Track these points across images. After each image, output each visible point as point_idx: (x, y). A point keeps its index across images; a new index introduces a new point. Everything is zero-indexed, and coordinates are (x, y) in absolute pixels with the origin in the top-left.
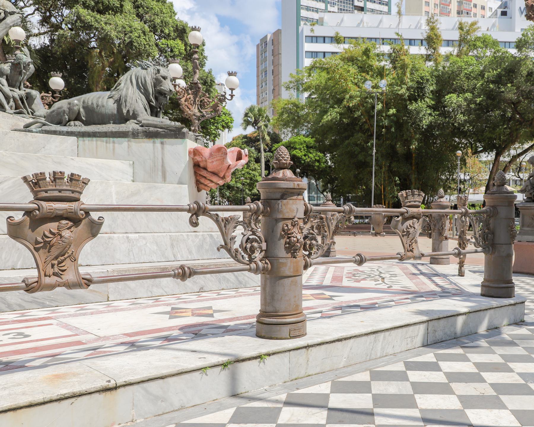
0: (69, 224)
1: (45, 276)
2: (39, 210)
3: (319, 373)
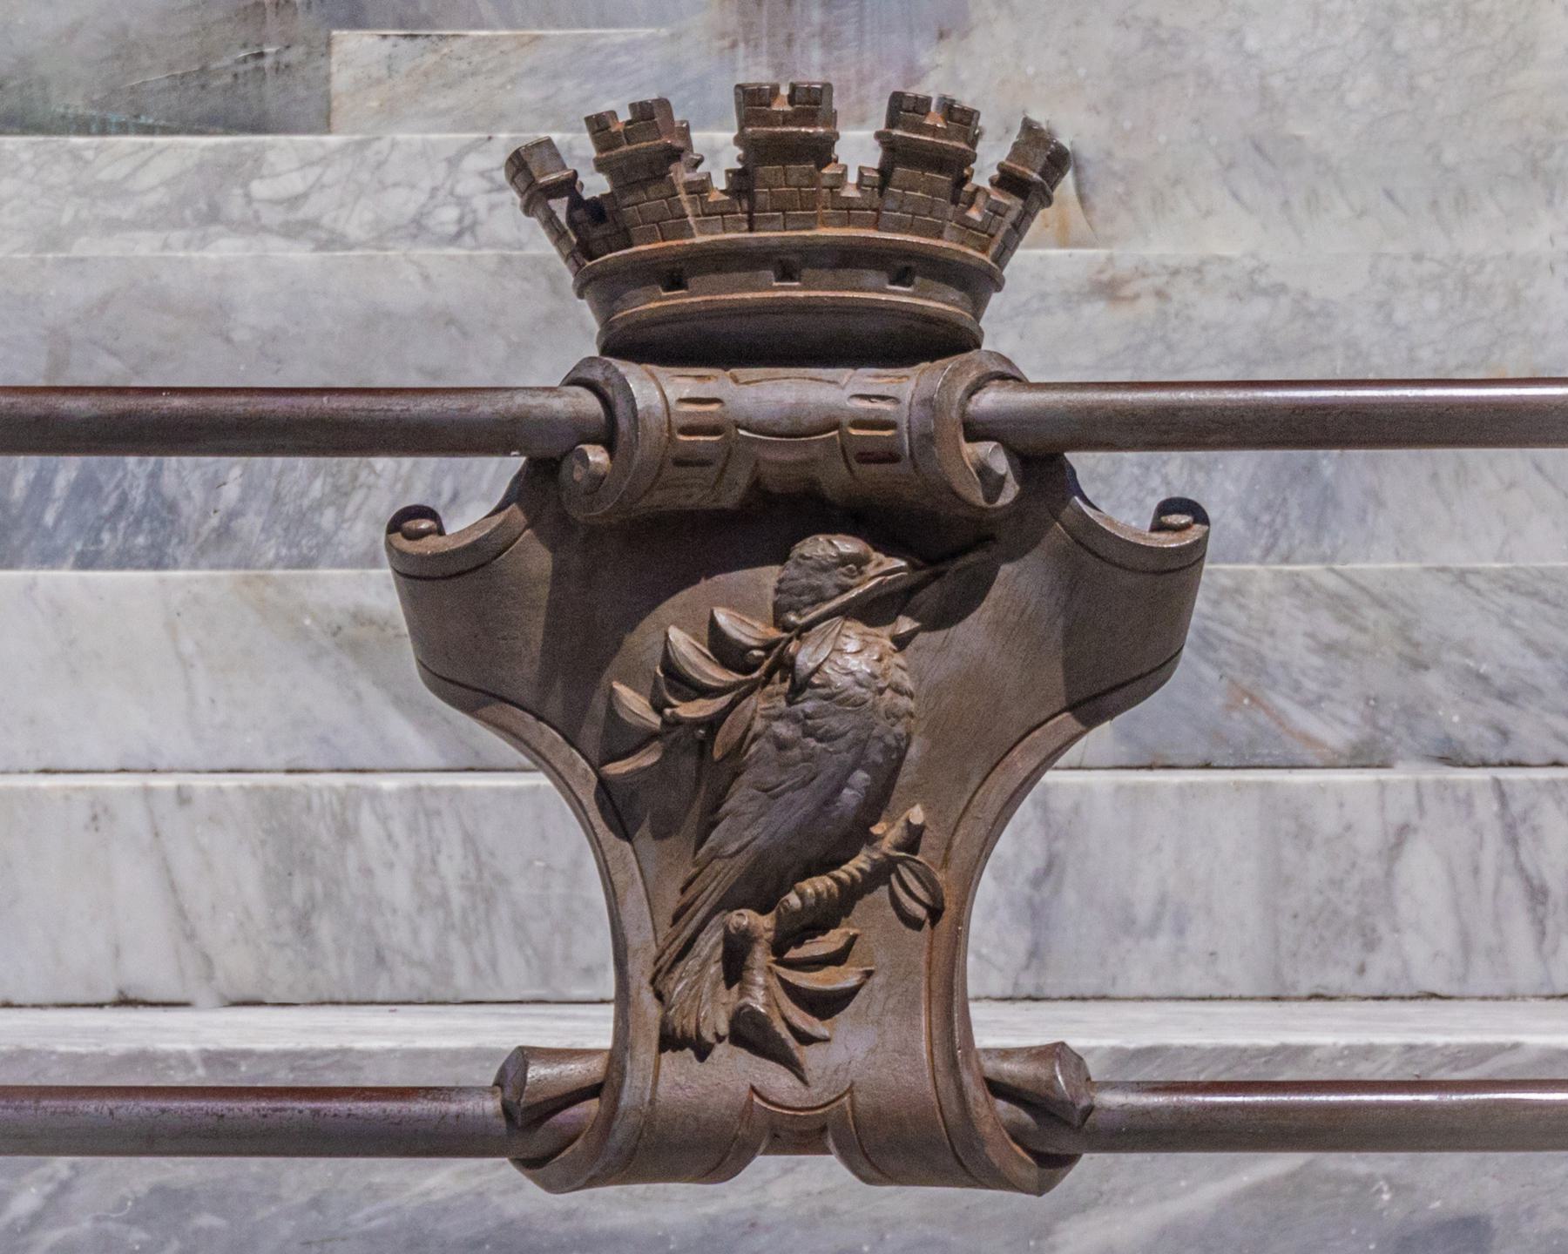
0: (870, 570)
1: (670, 1041)
2: (608, 437)
3: (829, 382)
